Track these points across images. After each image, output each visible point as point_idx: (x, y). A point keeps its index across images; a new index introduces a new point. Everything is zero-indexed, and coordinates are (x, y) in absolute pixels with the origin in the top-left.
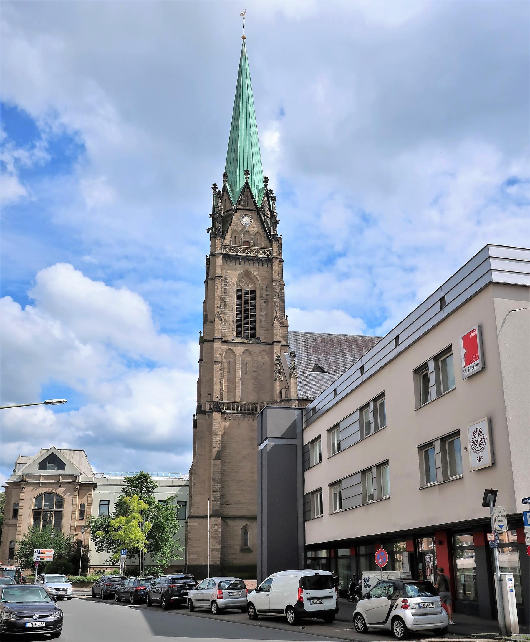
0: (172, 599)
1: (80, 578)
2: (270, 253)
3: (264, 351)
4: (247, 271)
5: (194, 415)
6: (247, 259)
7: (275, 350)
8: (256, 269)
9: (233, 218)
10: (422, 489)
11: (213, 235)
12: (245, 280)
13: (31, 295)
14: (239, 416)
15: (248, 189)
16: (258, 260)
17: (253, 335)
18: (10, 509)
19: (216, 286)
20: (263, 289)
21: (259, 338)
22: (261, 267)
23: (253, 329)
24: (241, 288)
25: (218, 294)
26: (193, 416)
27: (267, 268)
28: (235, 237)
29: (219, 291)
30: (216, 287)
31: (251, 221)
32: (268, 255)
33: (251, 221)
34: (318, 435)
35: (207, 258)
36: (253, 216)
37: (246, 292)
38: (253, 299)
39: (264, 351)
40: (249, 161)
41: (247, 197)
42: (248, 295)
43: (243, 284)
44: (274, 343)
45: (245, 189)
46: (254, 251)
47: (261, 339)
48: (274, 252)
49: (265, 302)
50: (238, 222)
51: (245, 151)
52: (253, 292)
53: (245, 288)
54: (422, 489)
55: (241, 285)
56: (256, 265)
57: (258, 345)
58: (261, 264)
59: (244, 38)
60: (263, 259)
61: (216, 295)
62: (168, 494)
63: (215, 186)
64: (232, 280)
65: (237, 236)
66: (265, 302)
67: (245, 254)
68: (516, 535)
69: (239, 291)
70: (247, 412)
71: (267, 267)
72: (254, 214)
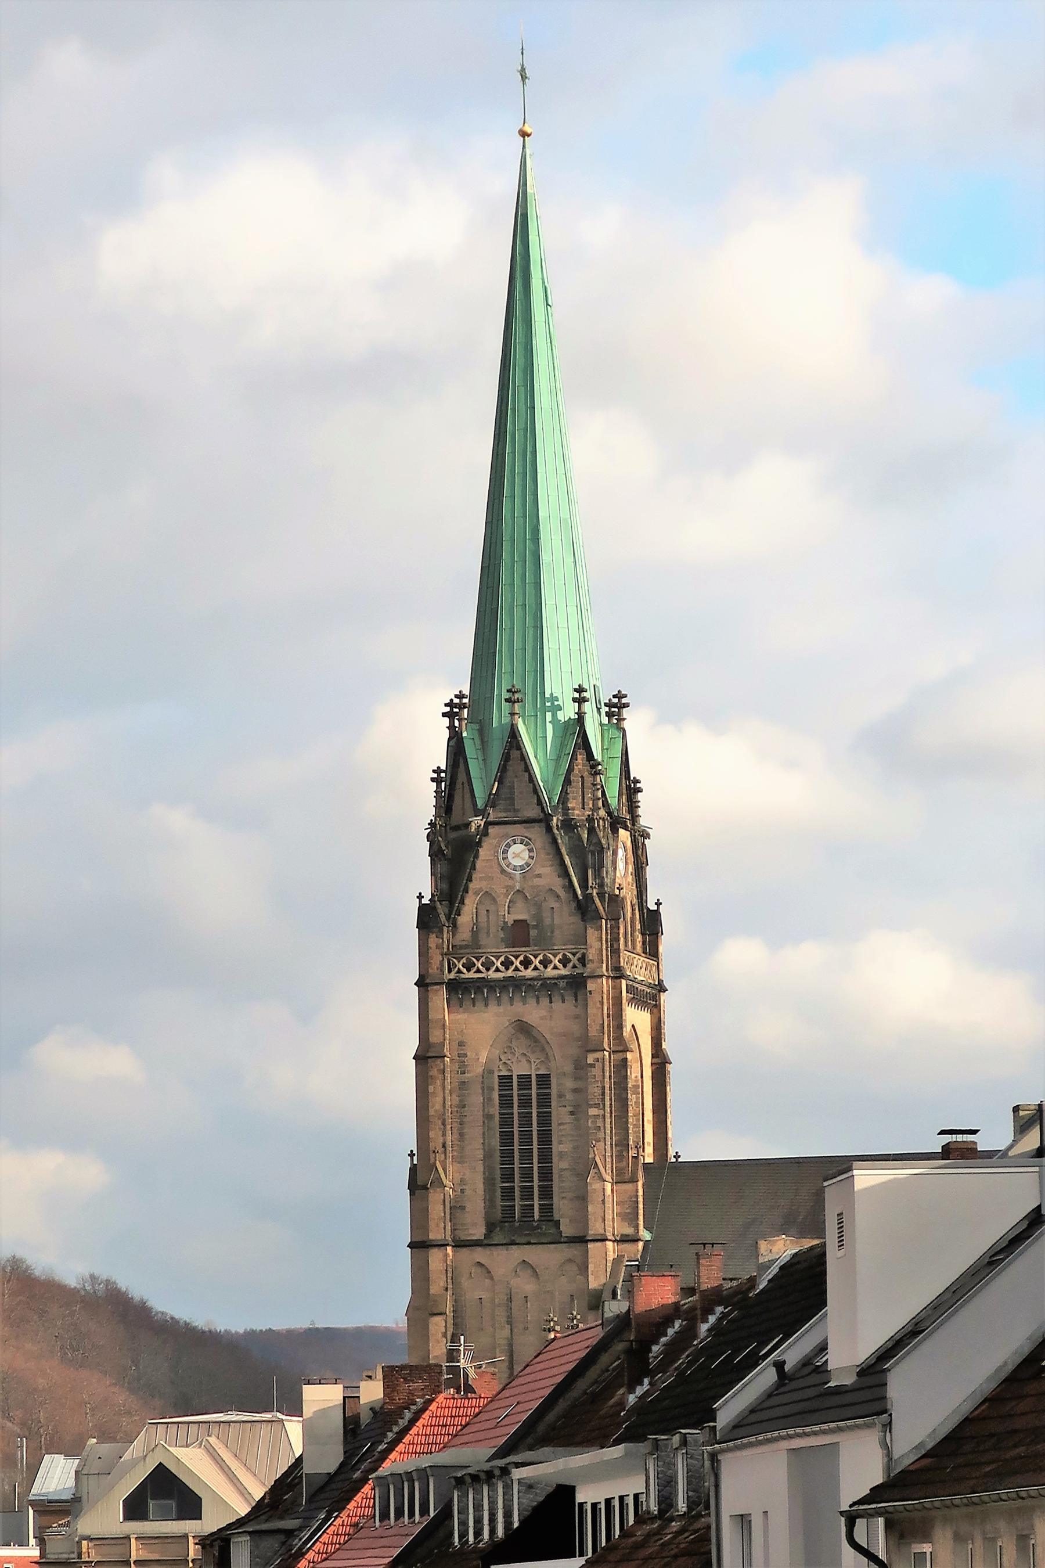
0: (459, 759)
2: (583, 960)
3: (570, 1261)
4: (518, 1022)
5: (412, 1151)
6: (515, 985)
7: (593, 1265)
8: (543, 1013)
9: (476, 856)
12: (520, 1046)
13: (145, 1301)
15: (531, 785)
16: (546, 988)
19: (431, 1085)
20: (564, 1074)
22: (557, 1005)
25: (436, 1111)
26: (418, 897)
27: (576, 1007)
29: (439, 1099)
30: (431, 1089)
31: (531, 854)
32: (574, 967)
33: (531, 854)
34: (628, 1494)
35: (420, 901)
36: (535, 840)
37: (525, 1081)
38: (545, 1101)
39: (570, 1261)
40: (530, 634)
42: (513, 1146)
43: (514, 1060)
45: (508, 754)
46: (536, 962)
47: (561, 1229)
48: (591, 957)
49: (572, 1113)
50: (491, 867)
51: (518, 601)
52: (544, 1080)
53: (519, 1069)
56: (545, 1001)
57: (554, 1245)
58: (556, 998)
59: (524, 134)
61: (432, 1112)
62: (713, 1246)
63: (420, 897)
64: (477, 1054)
65: (492, 908)
66: (572, 1113)
67: (510, 973)
71: (576, 1000)
72: (536, 833)
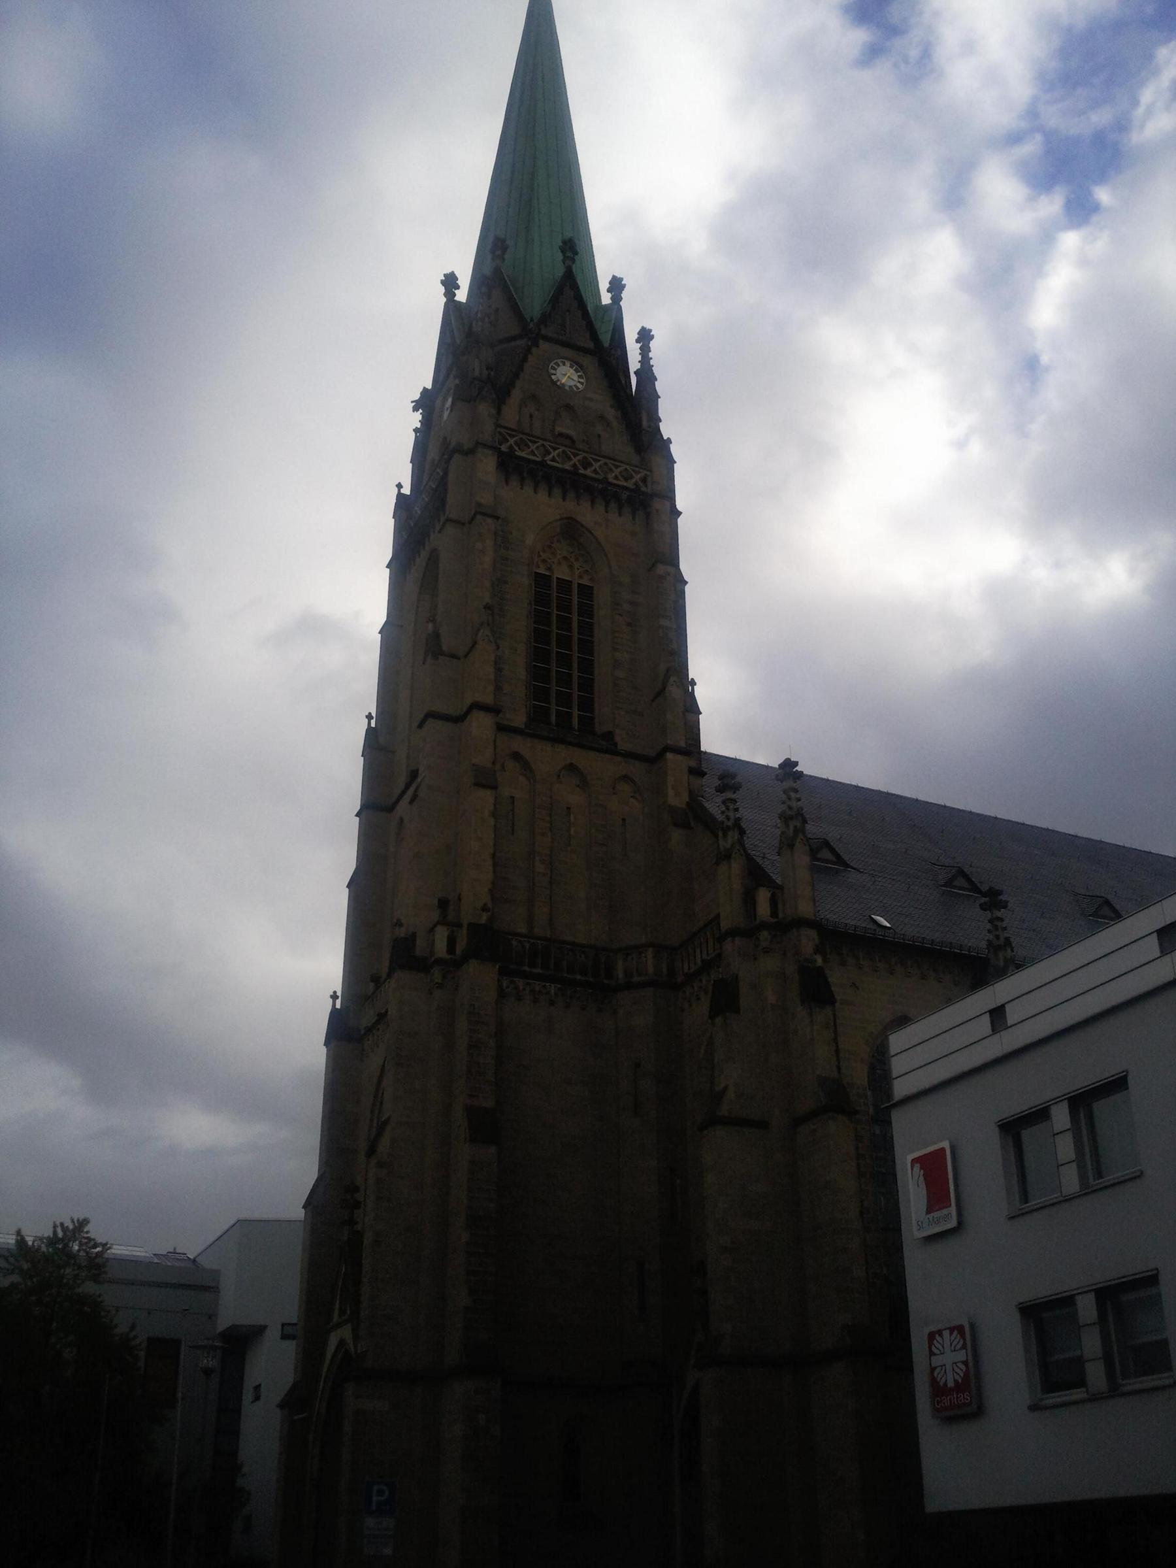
1: (533, 603)
3: (626, 778)
10: (1034, 1408)
11: (97, 1253)
14: (553, 991)
17: (587, 723)
18: (1153, 1375)
21: (609, 736)
23: (587, 705)
24: (549, 569)
28: (531, 416)
31: (582, 380)
37: (565, 586)
38: (587, 610)
39: (626, 778)
41: (568, 311)
44: (669, 756)
53: (561, 572)
54: (1034, 1408)
55: (549, 561)
58: (613, 505)
60: (624, 496)
66: (629, 624)
67: (567, 466)
68: (76, 1224)
69: (541, 581)
70: (579, 977)
